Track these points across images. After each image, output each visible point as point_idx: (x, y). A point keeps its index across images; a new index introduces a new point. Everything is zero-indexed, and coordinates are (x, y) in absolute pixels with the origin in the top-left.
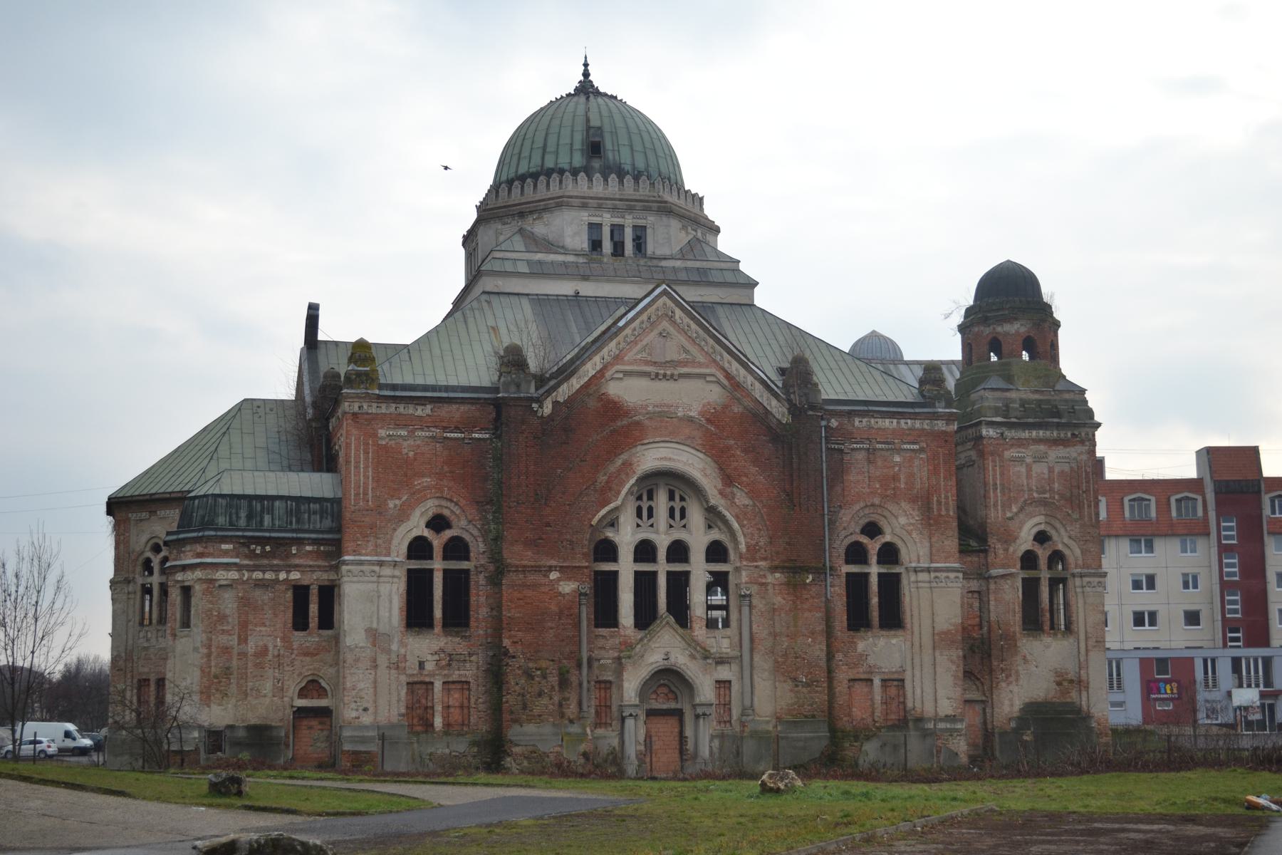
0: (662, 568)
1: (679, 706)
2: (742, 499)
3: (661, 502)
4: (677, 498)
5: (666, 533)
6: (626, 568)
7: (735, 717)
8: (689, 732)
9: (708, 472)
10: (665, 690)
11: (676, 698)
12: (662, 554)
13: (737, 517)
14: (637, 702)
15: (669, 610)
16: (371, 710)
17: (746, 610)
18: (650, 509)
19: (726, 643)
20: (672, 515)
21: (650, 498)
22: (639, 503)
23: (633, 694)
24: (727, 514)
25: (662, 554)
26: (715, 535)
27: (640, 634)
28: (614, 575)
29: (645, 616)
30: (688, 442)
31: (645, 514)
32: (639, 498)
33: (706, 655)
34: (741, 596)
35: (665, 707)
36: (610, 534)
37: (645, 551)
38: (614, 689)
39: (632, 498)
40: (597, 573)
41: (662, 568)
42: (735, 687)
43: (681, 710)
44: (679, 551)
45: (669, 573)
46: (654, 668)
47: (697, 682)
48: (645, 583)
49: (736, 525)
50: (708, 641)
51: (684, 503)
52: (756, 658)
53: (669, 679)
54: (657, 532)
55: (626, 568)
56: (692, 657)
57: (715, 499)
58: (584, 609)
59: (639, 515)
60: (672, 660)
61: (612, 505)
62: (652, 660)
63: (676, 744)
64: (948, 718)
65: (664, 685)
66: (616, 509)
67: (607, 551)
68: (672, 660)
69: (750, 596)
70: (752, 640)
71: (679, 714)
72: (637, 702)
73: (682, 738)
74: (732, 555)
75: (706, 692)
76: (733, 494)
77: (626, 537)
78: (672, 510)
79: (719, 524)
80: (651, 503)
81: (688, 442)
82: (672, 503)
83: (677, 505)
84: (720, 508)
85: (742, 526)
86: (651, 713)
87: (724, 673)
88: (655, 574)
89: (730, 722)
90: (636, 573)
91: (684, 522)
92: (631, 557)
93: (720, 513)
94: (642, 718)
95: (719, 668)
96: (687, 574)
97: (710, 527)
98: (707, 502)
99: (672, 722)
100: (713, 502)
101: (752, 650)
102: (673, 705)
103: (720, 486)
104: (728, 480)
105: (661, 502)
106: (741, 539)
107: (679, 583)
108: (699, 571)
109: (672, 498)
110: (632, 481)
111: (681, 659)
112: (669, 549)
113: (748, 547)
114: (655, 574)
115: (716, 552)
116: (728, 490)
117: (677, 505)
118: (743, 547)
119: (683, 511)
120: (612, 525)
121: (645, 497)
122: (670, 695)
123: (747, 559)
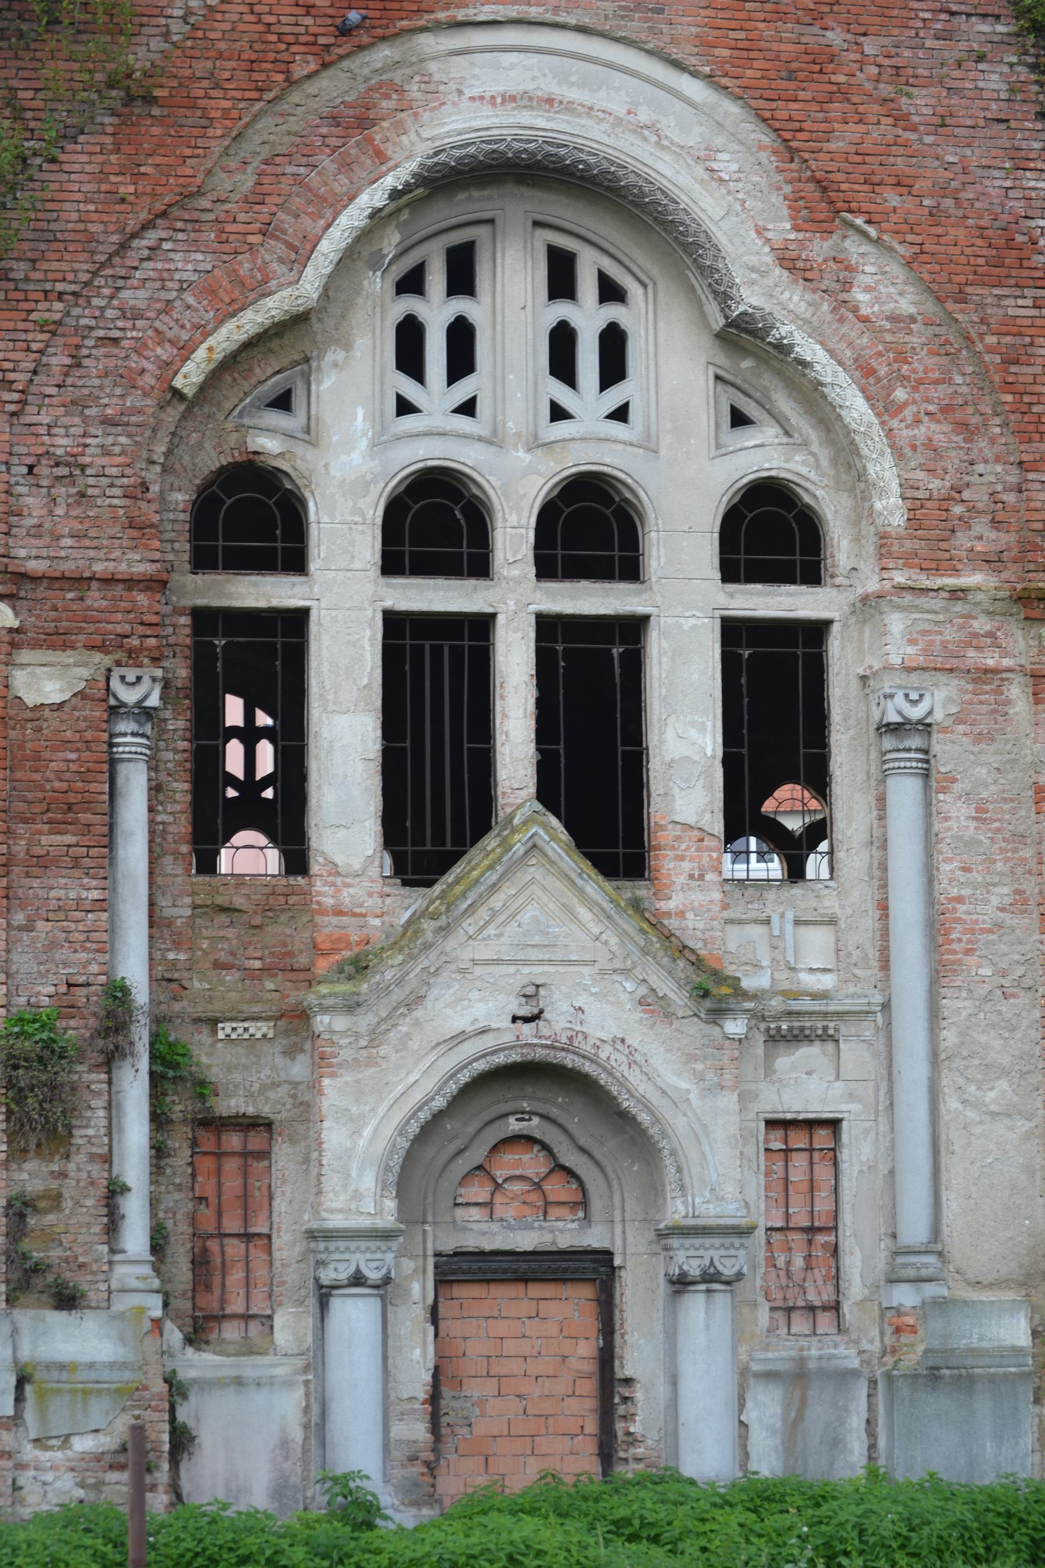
0: (515, 599)
1: (594, 1238)
2: (885, 286)
3: (512, 304)
4: (587, 286)
5: (535, 444)
6: (345, 600)
7: (855, 1288)
8: (637, 1359)
9: (727, 164)
10: (530, 1163)
11: (583, 1203)
12: (513, 538)
13: (864, 372)
14: (388, 1219)
15: (547, 793)
16: (213, 1200)
17: (904, 792)
18: (461, 339)
19: (816, 946)
20: (562, 361)
21: (462, 279)
22: (410, 304)
23: (368, 1182)
24: (807, 349)
25: (513, 538)
26: (761, 454)
27: (410, 902)
28: (287, 633)
29: (434, 817)
30: (634, 27)
31: (437, 354)
32: (412, 283)
33: (713, 992)
34: (894, 729)
35: (526, 1241)
36: (269, 441)
37: (432, 522)
38: (284, 1156)
39: (377, 285)
40: (206, 620)
41: (515, 599)
42: (858, 1150)
43: (606, 1256)
44: (589, 525)
45: (479, 566)
46: (472, 1057)
47: (679, 1124)
48: (432, 675)
49: (856, 408)
50: (734, 939)
51: (613, 312)
52: (957, 1005)
53: (535, 1095)
54: (493, 440)
55: (345, 600)
56: (652, 1004)
57: (762, 289)
58: (135, 783)
59: (410, 356)
60: (558, 1021)
61: (274, 307)
62: (460, 1022)
63: (583, 1410)
64: (273, 876)
65: (528, 1140)
66: (297, 322)
67: (255, 517)
68: (558, 1021)
69: (924, 727)
70: (937, 928)
71: (597, 1270)
72: (388, 1219)
73: (609, 1384)
74: (841, 546)
75: (718, 1172)
76: (846, 274)
77: (349, 454)
78: (562, 344)
79: (784, 404)
80: (461, 305)
81: (634, 27)
82: (562, 310)
83: (588, 318)
84: (785, 330)
85: (886, 409)
86: (458, 1270)
87: (805, 1084)
88: (482, 625)
89: (836, 1307)
90: (296, 562)
91: (615, 397)
92: (368, 547)
93: (783, 349)
94: (420, 1289)
95: (785, 1061)
96: (632, 629)
97: (739, 419)
98: (724, 298)
99: (571, 1306)
100: (750, 298)
101: (939, 975)
102: (566, 1234)
103: (782, 229)
104: (824, 201)
105: (512, 304)
106: (883, 469)
107: (595, 683)
108: (684, 612)
109: (561, 282)
110: (373, 197)
111: (601, 1008)
112: (549, 518)
113: (916, 509)
114: (482, 625)
115: (768, 532)
116: (819, 249)
117: (588, 318)
118: (890, 508)
119: (613, 345)
120: (283, 402)
121: (436, 280)
122: (558, 1189)
123: (908, 560)
